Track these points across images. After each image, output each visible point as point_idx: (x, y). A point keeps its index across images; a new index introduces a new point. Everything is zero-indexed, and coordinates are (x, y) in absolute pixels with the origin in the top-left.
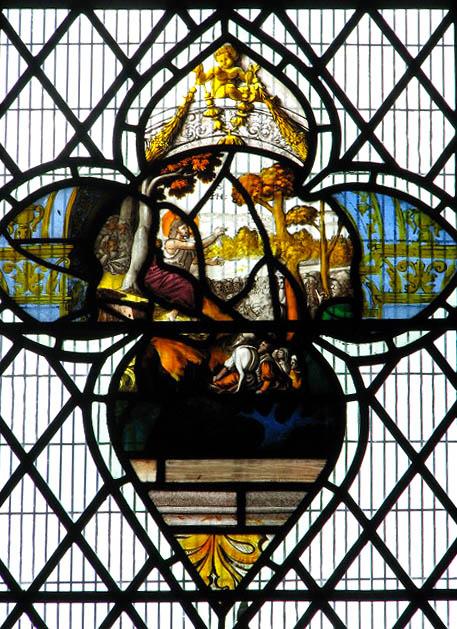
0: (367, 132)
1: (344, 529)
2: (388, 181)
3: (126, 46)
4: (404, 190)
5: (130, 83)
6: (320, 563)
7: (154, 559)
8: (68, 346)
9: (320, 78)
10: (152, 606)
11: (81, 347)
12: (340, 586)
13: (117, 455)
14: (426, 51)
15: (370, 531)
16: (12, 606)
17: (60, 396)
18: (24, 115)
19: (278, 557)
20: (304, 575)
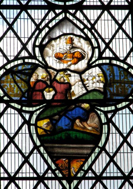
0: (107, 46)
1: (104, 159)
2: (114, 62)
4: (119, 64)
5: (37, 32)
6: (98, 168)
7: (49, 168)
8: (24, 108)
10: (50, 181)
11: (27, 109)
12: (104, 175)
13: (38, 139)
14: (124, 21)
15: (112, 159)
17: (21, 121)
19: (86, 167)
20: (94, 172)
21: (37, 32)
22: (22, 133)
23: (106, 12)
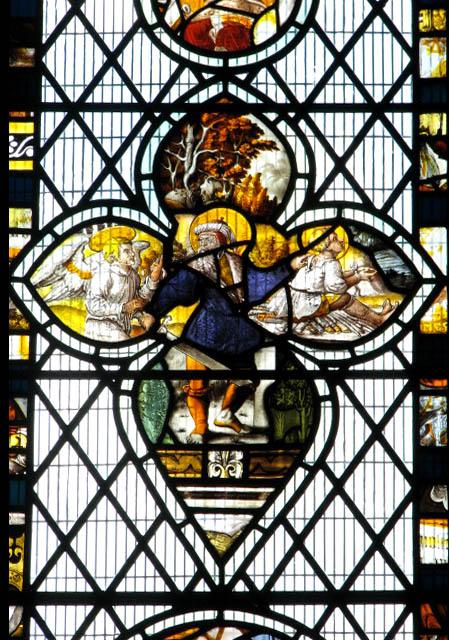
3: (269, 82)
5: (148, 125)
9: (290, 342)
16: (368, 115)
18: (102, 525)
21: (148, 125)
22: (67, 521)
23: (338, 611)
